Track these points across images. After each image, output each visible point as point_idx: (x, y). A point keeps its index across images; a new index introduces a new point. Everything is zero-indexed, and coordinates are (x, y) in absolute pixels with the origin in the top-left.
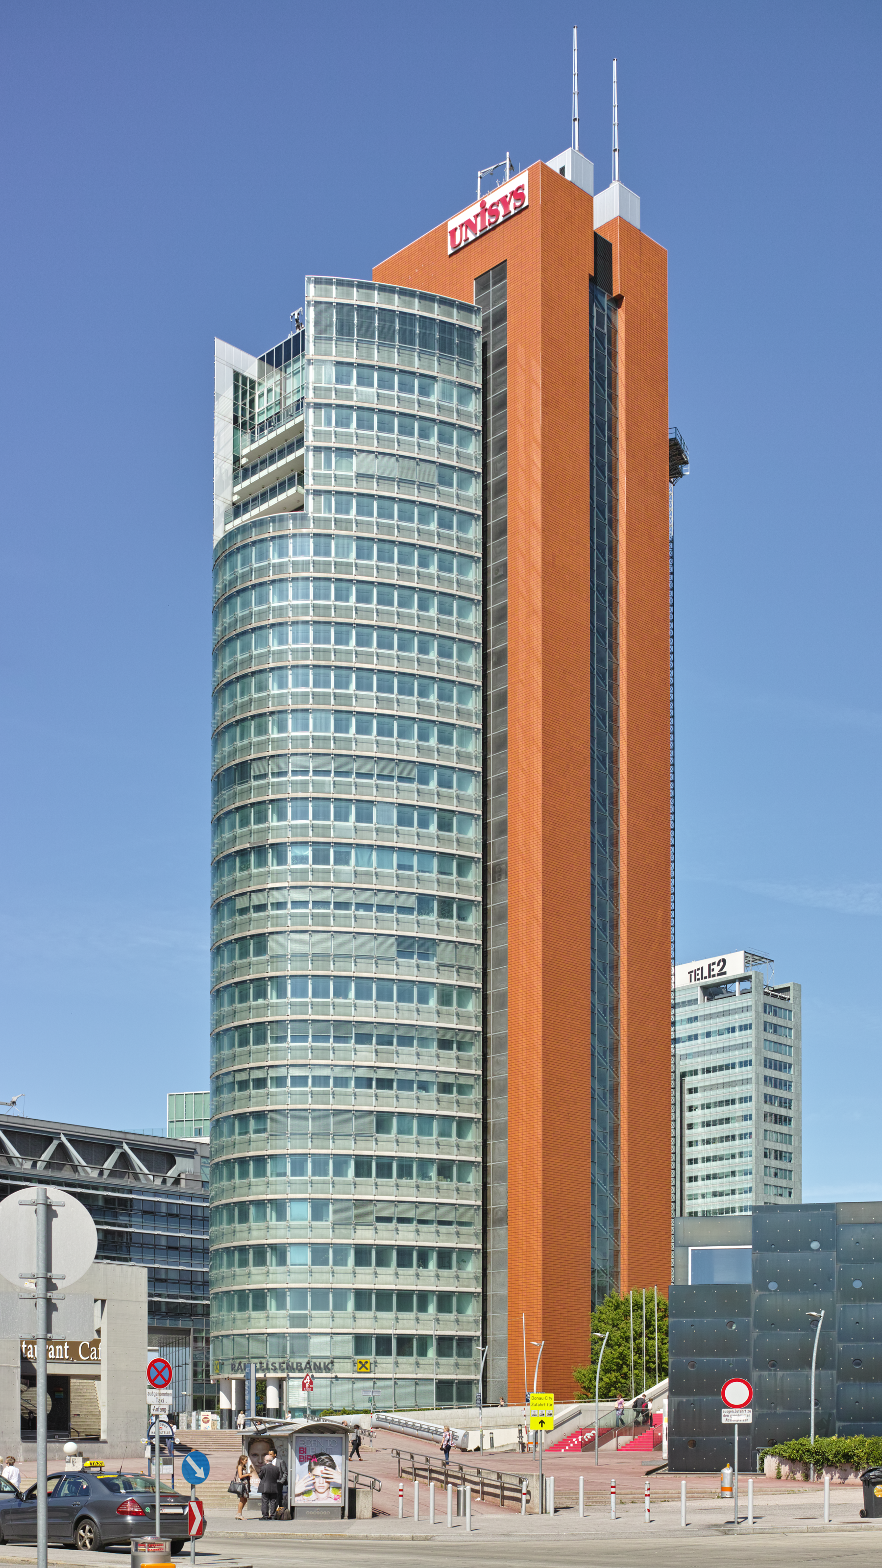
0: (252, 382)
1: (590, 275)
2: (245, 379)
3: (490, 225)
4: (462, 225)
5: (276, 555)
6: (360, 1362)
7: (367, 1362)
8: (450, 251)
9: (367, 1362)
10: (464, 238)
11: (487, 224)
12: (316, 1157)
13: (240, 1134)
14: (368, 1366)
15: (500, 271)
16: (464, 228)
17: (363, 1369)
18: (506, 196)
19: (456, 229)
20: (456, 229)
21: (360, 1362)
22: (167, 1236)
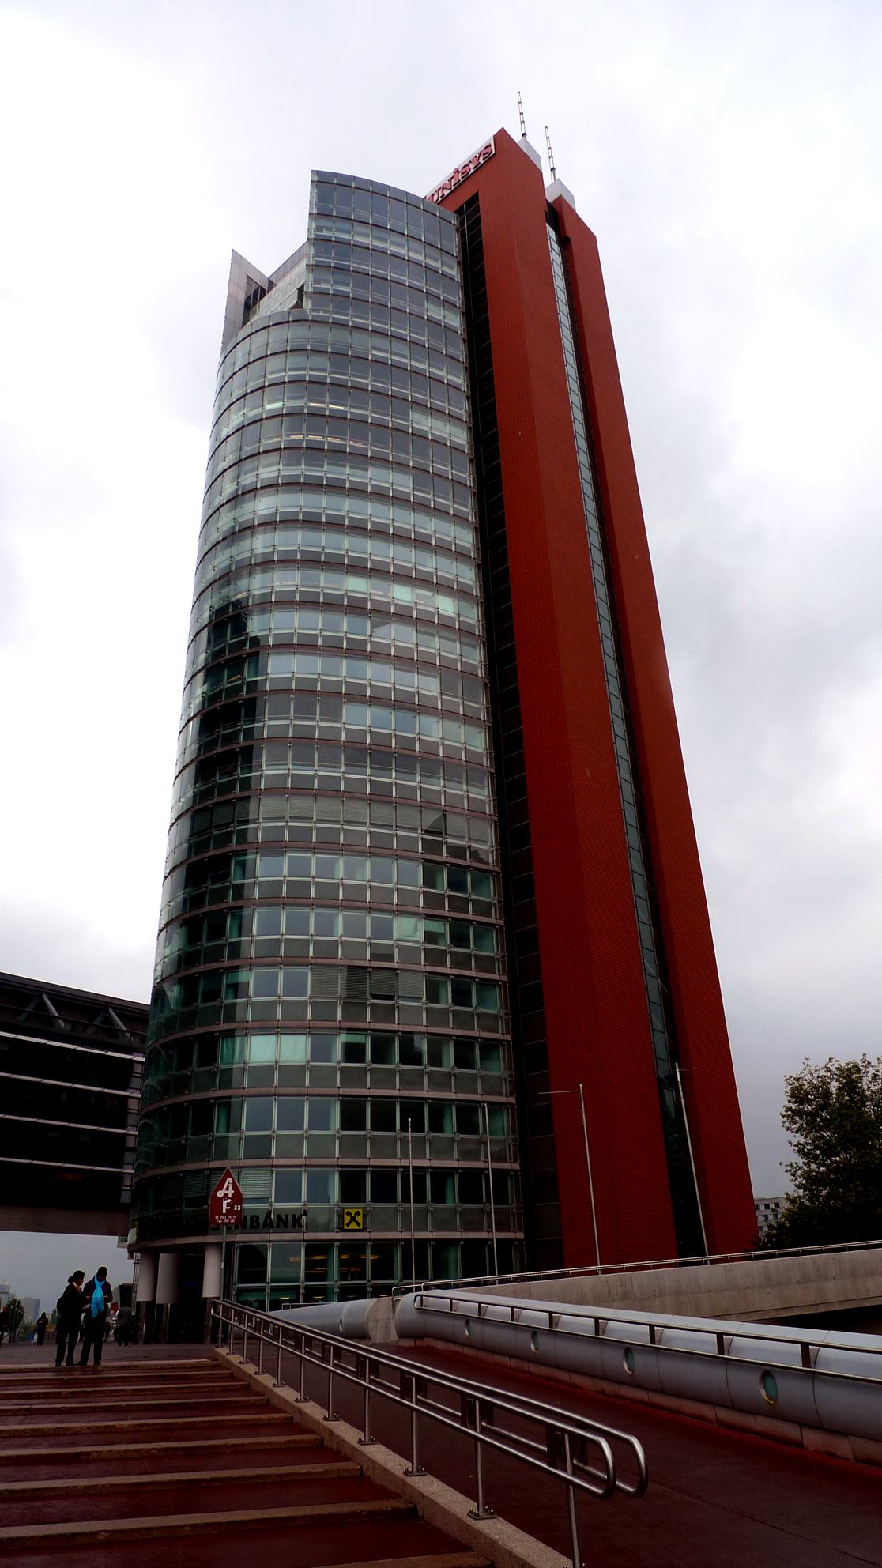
6: (349, 1214)
7: (358, 1213)
9: (358, 1213)
14: (359, 1219)
15: (474, 199)
21: (349, 1214)
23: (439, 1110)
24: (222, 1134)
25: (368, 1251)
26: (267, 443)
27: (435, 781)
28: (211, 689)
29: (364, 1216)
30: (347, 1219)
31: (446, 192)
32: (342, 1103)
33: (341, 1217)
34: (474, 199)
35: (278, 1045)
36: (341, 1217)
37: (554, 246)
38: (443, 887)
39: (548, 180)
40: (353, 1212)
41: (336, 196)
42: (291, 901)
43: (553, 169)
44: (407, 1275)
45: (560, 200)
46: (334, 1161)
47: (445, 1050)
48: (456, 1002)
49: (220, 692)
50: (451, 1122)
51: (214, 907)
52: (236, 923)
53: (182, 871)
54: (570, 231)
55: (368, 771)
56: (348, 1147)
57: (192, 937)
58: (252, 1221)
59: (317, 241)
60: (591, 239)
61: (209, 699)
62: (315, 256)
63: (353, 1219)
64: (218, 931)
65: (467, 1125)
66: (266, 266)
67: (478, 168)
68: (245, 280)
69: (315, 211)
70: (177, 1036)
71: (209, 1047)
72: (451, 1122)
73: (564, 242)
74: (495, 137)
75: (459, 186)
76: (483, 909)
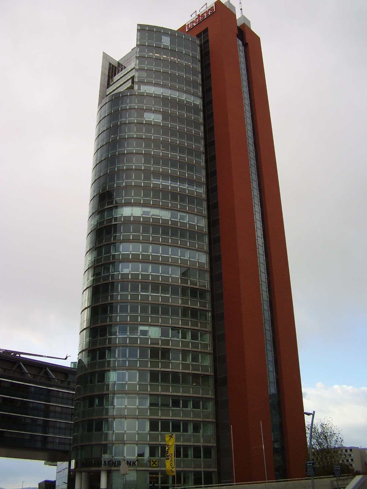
0: (116, 67)
1: (237, 34)
2: (113, 66)
3: (201, 20)
4: (191, 22)
5: (114, 251)
6: (152, 461)
7: (156, 461)
8: (187, 30)
9: (156, 461)
10: (192, 25)
11: (200, 19)
12: (185, 421)
13: (98, 382)
14: (156, 463)
15: (206, 31)
16: (192, 23)
17: (154, 465)
18: (207, 11)
19: (189, 24)
20: (189, 24)
21: (152, 461)
22: (59, 437)
23: (186, 423)
24: (106, 432)
25: (160, 474)
26: (103, 469)
27: (185, 185)
28: (100, 219)
29: (158, 462)
30: (152, 463)
31: (195, 24)
32: (150, 349)
33: (150, 462)
34: (206, 31)
35: (132, 210)
36: (150, 462)
37: (242, 48)
38: (189, 361)
39: (238, 16)
40: (154, 461)
41: (147, 33)
42: (133, 241)
43: (241, 9)
44: (174, 483)
45: (244, 25)
46: (148, 369)
47: (189, 404)
48: (192, 338)
49: (104, 221)
50: (191, 428)
51: (103, 303)
52: (114, 248)
53: (97, 197)
54: (248, 40)
55: (160, 293)
56: (153, 364)
57: (99, 254)
58: (118, 463)
59: (140, 46)
60: (257, 40)
61: (100, 223)
62: (140, 52)
63: (154, 463)
64: (103, 356)
65: (196, 428)
66: (117, 56)
67: (208, 16)
68: (108, 63)
69: (139, 43)
70: (88, 395)
71: (102, 376)
72: (191, 428)
73: (245, 45)
74: (216, 3)
75: (200, 23)
76: (205, 346)
